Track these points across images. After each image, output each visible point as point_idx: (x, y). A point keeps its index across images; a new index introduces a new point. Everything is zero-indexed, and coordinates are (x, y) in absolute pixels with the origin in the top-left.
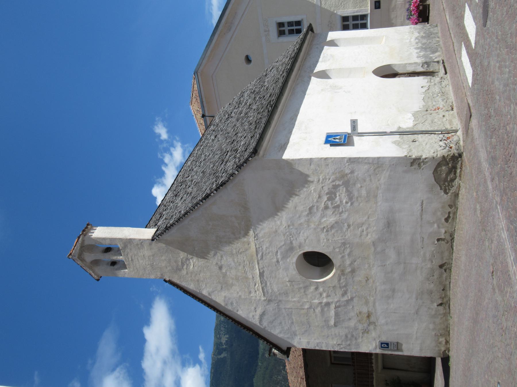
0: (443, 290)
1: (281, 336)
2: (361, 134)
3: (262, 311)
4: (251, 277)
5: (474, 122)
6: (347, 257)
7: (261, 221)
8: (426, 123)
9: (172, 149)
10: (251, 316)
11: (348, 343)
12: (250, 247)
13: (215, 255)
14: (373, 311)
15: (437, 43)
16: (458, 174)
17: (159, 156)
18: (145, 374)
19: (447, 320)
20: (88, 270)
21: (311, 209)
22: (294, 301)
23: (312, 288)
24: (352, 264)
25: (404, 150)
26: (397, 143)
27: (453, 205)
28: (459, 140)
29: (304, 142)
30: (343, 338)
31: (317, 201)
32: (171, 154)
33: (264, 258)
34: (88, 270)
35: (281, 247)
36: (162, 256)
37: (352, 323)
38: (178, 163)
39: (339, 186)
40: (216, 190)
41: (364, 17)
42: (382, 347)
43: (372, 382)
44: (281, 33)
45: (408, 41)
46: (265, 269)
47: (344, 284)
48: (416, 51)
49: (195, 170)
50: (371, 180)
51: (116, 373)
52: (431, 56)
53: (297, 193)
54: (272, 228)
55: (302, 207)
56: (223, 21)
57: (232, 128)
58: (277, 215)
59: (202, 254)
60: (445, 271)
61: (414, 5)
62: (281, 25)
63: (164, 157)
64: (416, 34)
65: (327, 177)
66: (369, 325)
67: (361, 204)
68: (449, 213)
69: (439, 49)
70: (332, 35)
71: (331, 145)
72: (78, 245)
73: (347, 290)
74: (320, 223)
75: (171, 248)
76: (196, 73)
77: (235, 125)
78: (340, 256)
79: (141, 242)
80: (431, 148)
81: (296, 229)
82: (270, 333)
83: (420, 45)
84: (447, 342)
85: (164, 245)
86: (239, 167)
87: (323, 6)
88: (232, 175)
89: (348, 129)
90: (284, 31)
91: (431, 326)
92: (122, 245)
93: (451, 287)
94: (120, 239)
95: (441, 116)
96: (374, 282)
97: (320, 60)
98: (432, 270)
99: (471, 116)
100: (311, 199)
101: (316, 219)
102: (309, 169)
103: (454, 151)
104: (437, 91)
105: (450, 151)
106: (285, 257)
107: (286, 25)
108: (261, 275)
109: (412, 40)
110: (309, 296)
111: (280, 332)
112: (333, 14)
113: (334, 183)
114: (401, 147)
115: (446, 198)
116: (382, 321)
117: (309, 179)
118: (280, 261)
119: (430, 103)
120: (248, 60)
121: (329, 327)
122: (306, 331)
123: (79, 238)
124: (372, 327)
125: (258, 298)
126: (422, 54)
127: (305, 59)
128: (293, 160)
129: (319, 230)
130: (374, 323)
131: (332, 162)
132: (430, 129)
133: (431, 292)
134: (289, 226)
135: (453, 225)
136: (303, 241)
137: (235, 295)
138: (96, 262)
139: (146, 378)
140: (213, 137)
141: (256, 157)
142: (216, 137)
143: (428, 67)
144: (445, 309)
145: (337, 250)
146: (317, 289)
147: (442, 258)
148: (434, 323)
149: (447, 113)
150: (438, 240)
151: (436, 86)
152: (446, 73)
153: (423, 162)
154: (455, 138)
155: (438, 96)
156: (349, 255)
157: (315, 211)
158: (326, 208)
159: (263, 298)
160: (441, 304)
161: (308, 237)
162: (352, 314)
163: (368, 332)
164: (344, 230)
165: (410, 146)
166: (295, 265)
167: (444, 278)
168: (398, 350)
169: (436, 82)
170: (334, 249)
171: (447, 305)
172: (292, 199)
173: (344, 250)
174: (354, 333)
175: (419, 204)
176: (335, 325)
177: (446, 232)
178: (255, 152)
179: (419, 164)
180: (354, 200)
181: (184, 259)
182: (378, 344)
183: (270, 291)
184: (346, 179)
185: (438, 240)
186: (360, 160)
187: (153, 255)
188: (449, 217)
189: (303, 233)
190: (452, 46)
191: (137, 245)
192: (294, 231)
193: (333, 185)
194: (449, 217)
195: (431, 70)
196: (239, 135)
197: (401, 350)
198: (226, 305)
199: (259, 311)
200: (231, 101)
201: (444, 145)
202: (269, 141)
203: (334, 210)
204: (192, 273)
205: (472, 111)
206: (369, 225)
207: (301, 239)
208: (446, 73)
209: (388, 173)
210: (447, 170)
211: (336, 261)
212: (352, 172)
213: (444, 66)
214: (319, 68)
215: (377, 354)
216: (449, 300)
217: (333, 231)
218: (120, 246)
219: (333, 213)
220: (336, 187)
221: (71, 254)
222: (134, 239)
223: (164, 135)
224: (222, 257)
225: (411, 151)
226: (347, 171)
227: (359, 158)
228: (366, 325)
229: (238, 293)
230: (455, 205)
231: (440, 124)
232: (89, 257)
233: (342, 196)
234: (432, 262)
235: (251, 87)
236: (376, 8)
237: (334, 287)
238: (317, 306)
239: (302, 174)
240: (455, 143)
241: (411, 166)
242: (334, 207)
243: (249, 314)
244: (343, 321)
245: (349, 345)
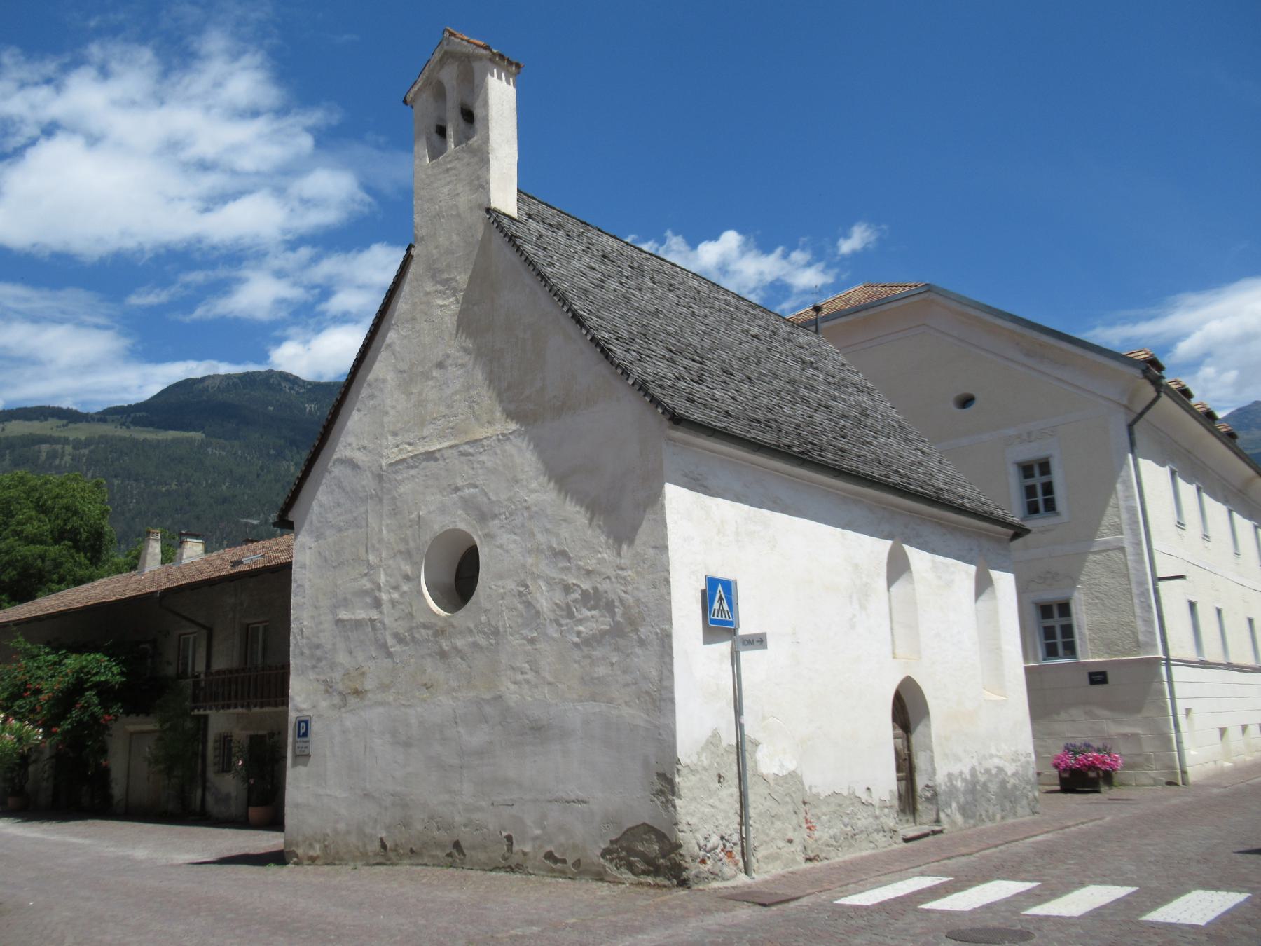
0: (412, 851)
1: (315, 506)
2: (735, 658)
3: (360, 464)
4: (426, 433)
5: (745, 913)
6: (471, 640)
7: (536, 446)
8: (769, 803)
9: (821, 265)
10: (351, 439)
11: (306, 651)
12: (482, 426)
13: (466, 350)
14: (366, 702)
15: (988, 817)
16: (643, 879)
17: (803, 240)
18: (360, 251)
19: (354, 859)
20: (423, 77)
21: (564, 554)
22: (381, 531)
23: (408, 569)
24: (457, 651)
25: (694, 758)
26: (713, 741)
27: (581, 870)
28: (724, 879)
29: (702, 530)
30: (315, 641)
31: (579, 568)
32: (809, 265)
33: (462, 459)
34: (423, 77)
35: (486, 494)
36: (458, 235)
37: (342, 658)
38: (789, 280)
39: (613, 614)
40: (593, 339)
41: (1070, 649)
43: (269, 705)
44: (1026, 470)
45: (993, 751)
46: (441, 463)
47: (417, 636)
48: (967, 772)
49: (671, 295)
50: (627, 685)
51: (361, 195)
52: (954, 805)
53: (595, 523)
54: (522, 470)
55: (567, 535)
56: (1045, 339)
57: (770, 371)
58: (549, 481)
59: (466, 323)
60: (449, 855)
61: (1097, 758)
62: (1045, 467)
63: (803, 249)
64: (1010, 769)
65: (630, 588)
66: (340, 693)
67: (576, 666)
68: (564, 861)
69: (972, 822)
70: (1005, 582)
71: (703, 593)
72: (471, 48)
73: (406, 644)
74: (536, 577)
75: (475, 252)
76: (929, 288)
77: (776, 377)
78: (472, 626)
79: (482, 186)
80: (702, 817)
81: (523, 526)
82: (318, 484)
83: (982, 778)
84: (313, 860)
85: (479, 236)
86: (642, 387)
87: (1091, 558)
88: (626, 373)
89: (746, 628)
90: (1032, 476)
91: (342, 826)
92: (476, 145)
93: (415, 868)
94: (488, 138)
95: (790, 835)
96: (424, 700)
97: (939, 558)
98: (450, 827)
99: (764, 905)
100: (584, 553)
101: (545, 567)
102: (644, 544)
103: (693, 869)
104: (859, 823)
105: (694, 860)
106: (467, 504)
107: (1045, 479)
108: (430, 456)
109: (996, 761)
110: (391, 562)
111: (321, 506)
112: (1073, 580)
113: (617, 604)
114: (702, 749)
115: (594, 854)
116: (350, 721)
117: (625, 547)
118: (460, 493)
119: (825, 809)
120: (966, 401)
121: (334, 608)
122: (326, 560)
123: (487, 48)
124: (337, 700)
125: (385, 452)
126: (959, 784)
127: (939, 523)
128: (663, 507)
129: (522, 575)
130: (345, 705)
131: (662, 597)
132: (752, 812)
133: (406, 824)
134: (528, 508)
135: (540, 869)
136: (499, 541)
137: (389, 402)
138: (440, 93)
139: (350, 256)
140: (755, 330)
141: (667, 423)
142: (756, 337)
143: (927, 799)
144: (376, 854)
145: (483, 618)
146: (407, 578)
147: (474, 848)
148: (348, 832)
149: (800, 848)
150: (509, 838)
151: (871, 820)
152: (906, 840)
153: (668, 801)
154: (728, 870)
155: (846, 826)
156: (475, 645)
157: (561, 565)
158: (567, 589)
159: (384, 462)
160: (384, 846)
161: (507, 551)
162: (360, 657)
163: (327, 691)
164: (523, 632)
165: (705, 769)
166: (451, 527)
167: (434, 853)
168: (296, 756)
169: (884, 820)
170: (486, 611)
171: (382, 860)
172: (583, 511)
173: (485, 633)
174: (324, 663)
175: (582, 795)
176: (339, 622)
177: (525, 854)
178: (677, 420)
179: (661, 793)
180: (585, 649)
181: (454, 284)
182: (307, 714)
183: (399, 477)
184: (628, 629)
185: (509, 838)
186: (667, 660)
187: (458, 215)
188: (556, 860)
189: (515, 541)
190: (964, 850)
191: (478, 178)
192: (518, 520)
193: (613, 601)
194: (556, 860)
195: (919, 807)
196: (745, 387)
197: (295, 764)
198: (370, 385)
199: (360, 457)
200: (852, 368)
201: (709, 846)
202: (713, 452)
203: (564, 606)
204: (428, 303)
205: (774, 908)
206: (536, 686)
207: (504, 538)
208: (906, 840)
209: (642, 724)
210: (652, 855)
211: (463, 617)
212: (642, 643)
213: (926, 835)
214: (918, 558)
215: (286, 714)
216: (392, 864)
217: (520, 607)
218: (475, 141)
219: (556, 604)
220: (610, 607)
221: (452, 34)
222: (488, 170)
223: (846, 247)
224: (463, 366)
225: (693, 772)
226: (643, 631)
227: (671, 657)
228: (340, 687)
229: (393, 407)
230: (580, 873)
231: (767, 835)
232: (449, 76)
233: (592, 622)
234: (465, 826)
235: (881, 408)
236: (1091, 675)
237: (411, 615)
238: (373, 582)
239: (635, 529)
240: (716, 870)
241: (658, 775)
242: (568, 606)
243: (355, 436)
244: (347, 639)
245: (302, 654)
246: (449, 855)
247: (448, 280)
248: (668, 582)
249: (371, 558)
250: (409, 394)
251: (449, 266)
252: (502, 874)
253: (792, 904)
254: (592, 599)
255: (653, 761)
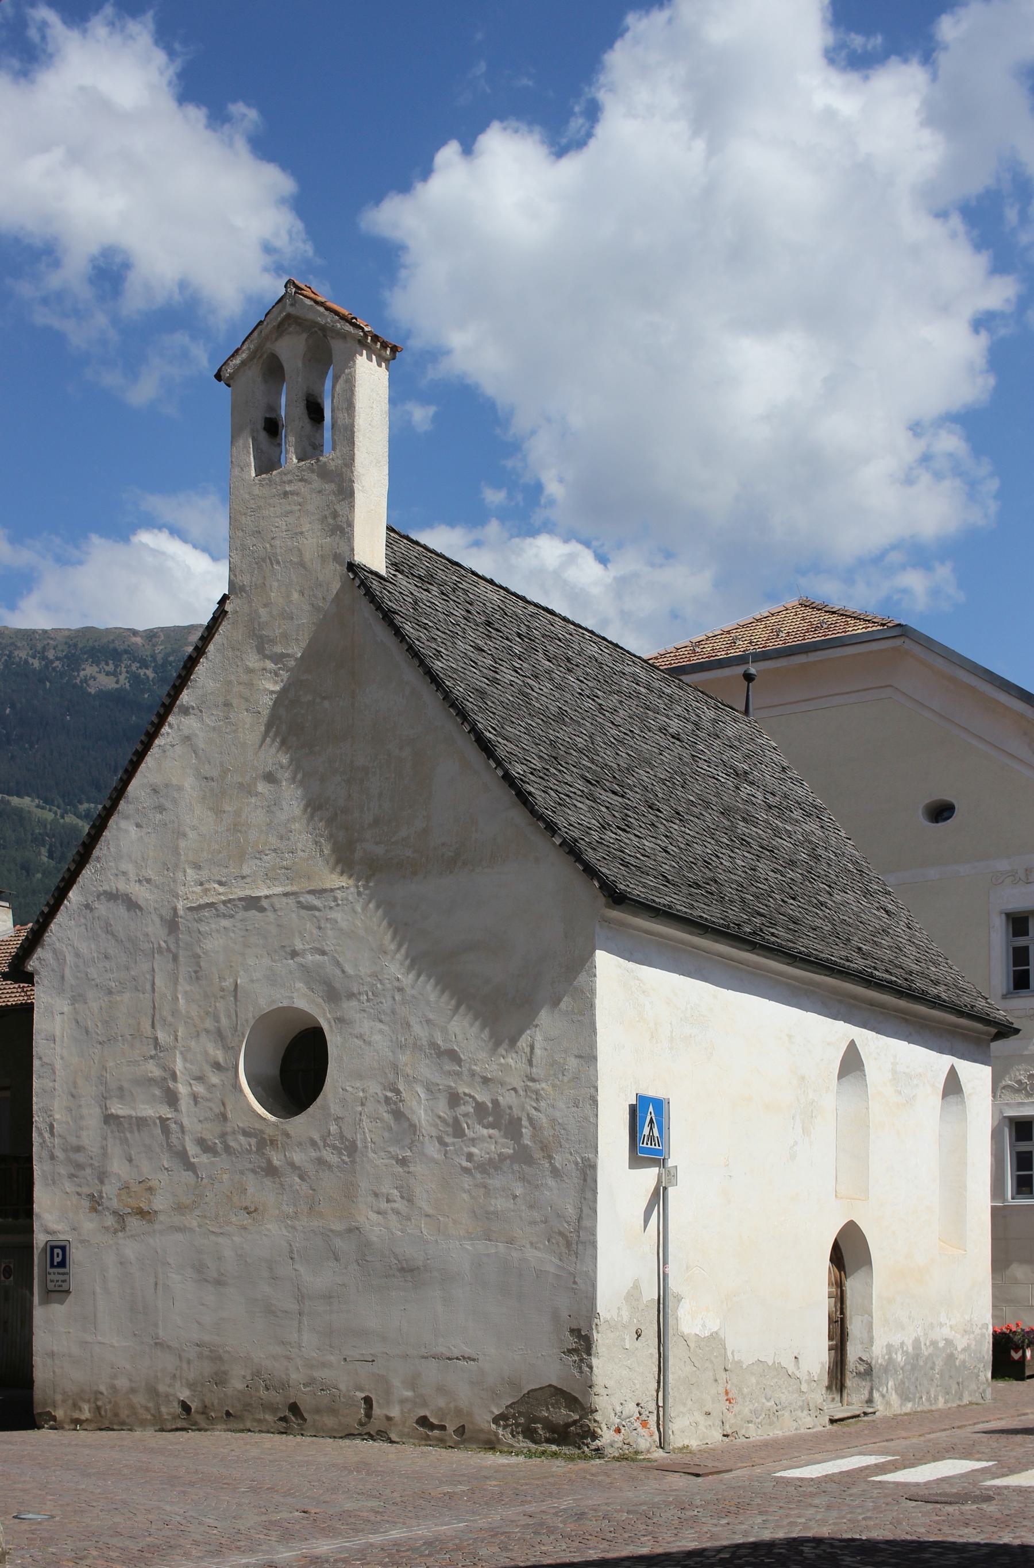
6: (314, 1154)
11: (59, 1153)
14: (157, 1227)
16: (545, 1446)
21: (453, 1056)
23: (220, 1056)
26: (633, 1295)
27: (465, 1436)
30: (73, 1141)
31: (473, 1074)
33: (303, 912)
35: (338, 964)
42: (52, 1248)
46: (271, 915)
47: (232, 1144)
50: (532, 1223)
52: (891, 1383)
66: (115, 1213)
67: (465, 1196)
74: (411, 1080)
77: (708, 805)
78: (316, 1137)
79: (341, 528)
80: (619, 1382)
86: (572, 850)
95: (708, 1408)
98: (284, 1386)
101: (426, 1070)
106: (308, 974)
108: (253, 903)
109: (946, 1332)
115: (483, 1419)
116: (130, 1250)
118: (299, 959)
121: (103, 1099)
124: (110, 1221)
125: (181, 890)
126: (899, 1358)
130: (123, 1229)
131: (586, 1118)
132: (671, 1378)
133: (220, 1379)
140: (675, 726)
141: (602, 900)
142: (676, 737)
143: (859, 1374)
146: (217, 1066)
147: (318, 1411)
148: (133, 1391)
151: (796, 1395)
152: (832, 1421)
153: (582, 1360)
156: (321, 1162)
157: (447, 1068)
162: (146, 1168)
164: (391, 1149)
165: (624, 1327)
166: (285, 1004)
173: (334, 1147)
175: (468, 1351)
176: (109, 1119)
177: (389, 1419)
178: (617, 898)
182: (62, 1237)
183: (204, 928)
184: (538, 1155)
185: (368, 1401)
187: (302, 564)
188: (432, 1427)
189: (381, 1031)
191: (335, 515)
194: (432, 1427)
195: (848, 1383)
199: (141, 893)
203: (450, 1121)
204: (250, 685)
207: (365, 1025)
208: (832, 1421)
209: (552, 1269)
210: (556, 1419)
211: (300, 1124)
222: (352, 507)
227: (594, 1191)
228: (115, 1204)
229: (194, 828)
230: (463, 1442)
233: (487, 1142)
237: (224, 1117)
241: (572, 1331)
242: (456, 1120)
244: (125, 1141)
245: (52, 1157)
246: (284, 1419)
247: (283, 656)
248: (594, 1101)
249: (161, 1036)
250: (218, 812)
251: (285, 636)
252: (358, 1441)
253: (726, 1476)
254: (491, 1114)
255: (564, 1314)
